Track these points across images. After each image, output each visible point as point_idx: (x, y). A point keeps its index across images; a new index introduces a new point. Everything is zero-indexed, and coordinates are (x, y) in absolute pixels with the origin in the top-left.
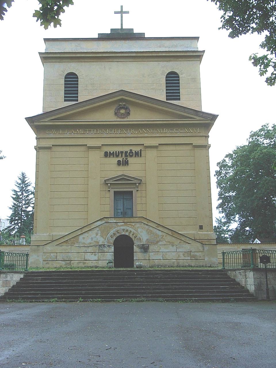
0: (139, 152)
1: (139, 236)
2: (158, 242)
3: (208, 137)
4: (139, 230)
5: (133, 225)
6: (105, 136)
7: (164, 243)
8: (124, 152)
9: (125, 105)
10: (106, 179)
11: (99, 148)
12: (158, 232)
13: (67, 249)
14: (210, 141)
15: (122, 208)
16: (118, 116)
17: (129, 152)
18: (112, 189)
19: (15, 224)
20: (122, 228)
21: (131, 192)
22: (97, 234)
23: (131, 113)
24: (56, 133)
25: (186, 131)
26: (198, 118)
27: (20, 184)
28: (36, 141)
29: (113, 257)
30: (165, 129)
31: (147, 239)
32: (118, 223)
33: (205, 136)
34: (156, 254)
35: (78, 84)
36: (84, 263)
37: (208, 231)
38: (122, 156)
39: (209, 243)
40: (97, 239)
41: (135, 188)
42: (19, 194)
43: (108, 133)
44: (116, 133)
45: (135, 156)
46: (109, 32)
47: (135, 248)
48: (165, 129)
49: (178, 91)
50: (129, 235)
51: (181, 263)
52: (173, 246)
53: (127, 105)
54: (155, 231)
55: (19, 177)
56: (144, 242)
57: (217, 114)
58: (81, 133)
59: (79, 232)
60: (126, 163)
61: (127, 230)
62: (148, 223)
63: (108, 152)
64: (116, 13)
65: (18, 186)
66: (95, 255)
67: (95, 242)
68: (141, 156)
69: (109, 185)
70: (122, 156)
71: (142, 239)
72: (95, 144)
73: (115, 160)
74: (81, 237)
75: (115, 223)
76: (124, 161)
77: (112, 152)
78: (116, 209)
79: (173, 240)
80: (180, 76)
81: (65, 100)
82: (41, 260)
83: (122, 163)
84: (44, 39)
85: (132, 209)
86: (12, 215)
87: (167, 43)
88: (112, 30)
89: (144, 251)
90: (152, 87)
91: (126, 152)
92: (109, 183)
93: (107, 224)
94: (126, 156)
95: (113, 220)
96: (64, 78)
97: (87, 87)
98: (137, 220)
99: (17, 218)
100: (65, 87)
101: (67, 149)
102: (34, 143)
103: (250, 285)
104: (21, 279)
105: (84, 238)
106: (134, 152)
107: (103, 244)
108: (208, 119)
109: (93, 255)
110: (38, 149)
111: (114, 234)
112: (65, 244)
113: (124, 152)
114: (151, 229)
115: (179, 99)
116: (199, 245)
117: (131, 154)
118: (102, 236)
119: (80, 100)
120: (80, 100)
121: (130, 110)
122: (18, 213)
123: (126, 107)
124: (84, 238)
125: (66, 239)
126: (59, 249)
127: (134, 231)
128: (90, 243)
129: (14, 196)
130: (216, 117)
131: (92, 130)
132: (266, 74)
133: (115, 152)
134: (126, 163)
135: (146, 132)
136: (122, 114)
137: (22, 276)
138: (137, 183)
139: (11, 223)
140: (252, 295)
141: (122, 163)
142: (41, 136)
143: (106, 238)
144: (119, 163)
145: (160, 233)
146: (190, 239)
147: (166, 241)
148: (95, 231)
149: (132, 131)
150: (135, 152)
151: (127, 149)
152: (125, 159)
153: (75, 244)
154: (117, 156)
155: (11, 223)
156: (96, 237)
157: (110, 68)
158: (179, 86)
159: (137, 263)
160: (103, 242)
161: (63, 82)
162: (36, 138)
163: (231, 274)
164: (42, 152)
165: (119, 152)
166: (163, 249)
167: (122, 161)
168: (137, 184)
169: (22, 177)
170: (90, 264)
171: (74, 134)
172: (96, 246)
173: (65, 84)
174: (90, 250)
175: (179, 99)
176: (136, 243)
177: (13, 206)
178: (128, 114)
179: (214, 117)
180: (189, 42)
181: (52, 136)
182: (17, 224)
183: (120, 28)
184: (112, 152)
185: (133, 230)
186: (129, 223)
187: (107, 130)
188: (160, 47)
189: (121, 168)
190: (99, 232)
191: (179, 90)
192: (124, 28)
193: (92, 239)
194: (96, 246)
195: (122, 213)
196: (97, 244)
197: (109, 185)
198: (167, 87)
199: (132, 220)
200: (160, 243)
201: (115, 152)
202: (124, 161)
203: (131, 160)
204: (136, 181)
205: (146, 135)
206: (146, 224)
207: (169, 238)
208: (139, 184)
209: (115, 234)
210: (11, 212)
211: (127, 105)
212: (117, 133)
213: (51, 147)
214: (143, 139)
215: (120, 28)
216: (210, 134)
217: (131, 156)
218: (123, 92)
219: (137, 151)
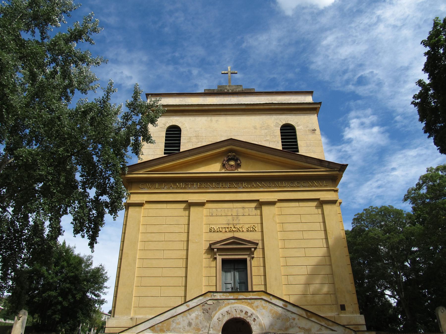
9: (235, 156)
10: (211, 242)
16: (226, 168)
18: (220, 256)
21: (245, 261)
23: (242, 164)
24: (150, 187)
30: (284, 182)
43: (214, 187)
44: (224, 186)
48: (284, 182)
49: (297, 150)
53: (237, 156)
58: (181, 187)
72: (198, 200)
81: (164, 154)
89: (331, 242)
90: (265, 139)
92: (215, 248)
96: (165, 131)
97: (190, 139)
101: (164, 206)
108: (335, 170)
119: (181, 150)
120: (181, 150)
121: (241, 161)
123: (236, 158)
130: (346, 167)
131: (195, 183)
132: (420, 83)
138: (253, 248)
146: (162, 323)
149: (244, 185)
157: (217, 121)
161: (164, 135)
168: (252, 249)
173: (166, 137)
204: (249, 246)
211: (237, 156)
212: (226, 186)
213: (143, 203)
218: (231, 141)
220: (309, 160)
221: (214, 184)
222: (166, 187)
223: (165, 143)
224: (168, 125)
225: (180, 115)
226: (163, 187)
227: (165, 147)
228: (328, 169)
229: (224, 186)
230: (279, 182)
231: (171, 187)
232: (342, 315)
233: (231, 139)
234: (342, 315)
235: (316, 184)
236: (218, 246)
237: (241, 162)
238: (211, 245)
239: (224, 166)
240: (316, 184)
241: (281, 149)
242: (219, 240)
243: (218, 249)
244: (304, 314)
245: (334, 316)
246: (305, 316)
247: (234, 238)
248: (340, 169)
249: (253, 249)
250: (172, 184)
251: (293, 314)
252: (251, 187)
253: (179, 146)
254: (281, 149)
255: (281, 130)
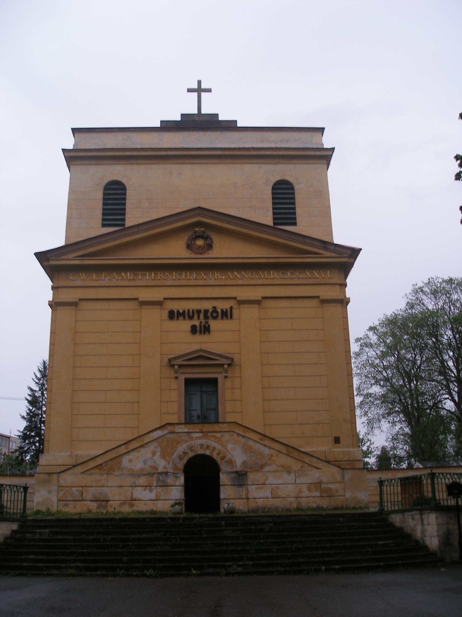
0: (229, 310)
1: (228, 457)
2: (262, 467)
3: (345, 285)
4: (230, 446)
5: (218, 438)
6: (170, 283)
7: (274, 467)
8: (203, 311)
9: (204, 232)
11: (159, 303)
12: (262, 448)
13: (100, 480)
14: (349, 292)
15: (198, 408)
16: (192, 251)
17: (210, 311)
19: (30, 443)
20: (199, 442)
21: (214, 382)
22: (154, 454)
24: (85, 278)
25: (308, 276)
26: (327, 254)
27: (39, 379)
28: (52, 292)
29: (183, 494)
30: (272, 272)
31: (244, 462)
32: (192, 434)
33: (341, 285)
34: (259, 488)
35: (125, 199)
36: (132, 505)
37: (348, 447)
38: (199, 317)
39: (351, 467)
40: (155, 462)
41: (221, 373)
42: (38, 394)
45: (222, 318)
46: (179, 118)
47: (224, 478)
50: (211, 455)
51: (304, 502)
52: (289, 472)
53: (208, 233)
54: (258, 447)
55: (39, 368)
56: (238, 466)
57: (361, 248)
59: (123, 450)
60: (206, 330)
61: (208, 446)
62: (244, 432)
63: (176, 311)
64: (189, 90)
65: (37, 381)
66: (151, 491)
67: (151, 467)
68: (231, 317)
69: (176, 367)
70: (199, 317)
71: (234, 463)
73: (186, 325)
74: (125, 460)
75: (186, 434)
76: (202, 325)
77: (181, 311)
78: (188, 410)
79: (289, 461)
80: (296, 187)
81: (104, 225)
82: (55, 499)
83: (198, 329)
84: (72, 129)
85: (216, 410)
86: (26, 428)
87: (273, 136)
88: (183, 115)
91: (206, 311)
92: (176, 365)
93: (172, 436)
94: (206, 317)
95: (182, 428)
98: (225, 427)
99: (33, 434)
100: (104, 204)
101: (105, 305)
102: (49, 296)
103: (431, 537)
104: (13, 531)
105: (130, 461)
106: (219, 311)
107: (166, 471)
109: (147, 491)
110: (53, 305)
111: (185, 453)
112: (97, 471)
113: (203, 311)
114: (251, 443)
115: (295, 224)
116: (335, 470)
117: (215, 315)
118: (163, 456)
119: (128, 223)
120: (128, 223)
122: (36, 427)
124: (130, 461)
125: (99, 461)
126: (87, 480)
127: (220, 447)
128: (142, 470)
129: (30, 398)
131: (148, 273)
133: (186, 311)
134: (206, 330)
135: (239, 277)
136: (200, 247)
137: (15, 526)
138: (226, 364)
139: (24, 442)
140: (434, 554)
141: (198, 329)
142: (62, 283)
143: (170, 460)
144: (194, 330)
145: (266, 451)
147: (277, 465)
148: (152, 447)
149: (216, 277)
150: (222, 310)
151: (208, 305)
152: (203, 322)
153: (114, 471)
154: (191, 318)
155: (24, 442)
156: (152, 459)
158: (294, 203)
159: (224, 506)
160: (165, 468)
162: (53, 288)
163: (367, 442)
164: (61, 310)
165: (193, 311)
166: (272, 480)
167: (198, 326)
169: (42, 367)
170: (141, 507)
171: (117, 280)
172: (151, 475)
174: (142, 481)
175: (295, 224)
176: (224, 467)
177: (28, 414)
178: (210, 247)
179: (333, 149)
180: (308, 135)
181: (79, 283)
182: (34, 443)
183: (196, 112)
184: (181, 311)
185: (218, 447)
186: (213, 434)
187: (173, 273)
188: (262, 141)
189: (198, 338)
190: (159, 449)
191: (294, 209)
192: (203, 112)
193: (145, 462)
194: (151, 475)
195: (198, 417)
196: (154, 471)
197: (176, 367)
198: (273, 204)
199: (216, 427)
200: (267, 468)
201: (186, 311)
202: (202, 325)
203: (213, 324)
204: (223, 361)
205: (240, 282)
206: (241, 435)
207: (284, 460)
208: (229, 365)
209: (186, 453)
210: (24, 424)
211: (208, 233)
214: (235, 288)
215: (196, 112)
216: (348, 280)
217: (215, 318)
219: (225, 310)
220: (307, 241)
221: (174, 274)
222: (106, 279)
223: (104, 209)
224: (106, 181)
225: (122, 164)
226: (103, 278)
227: (104, 214)
228: (334, 255)
229: (188, 277)
230: (266, 272)
231: (114, 279)
232: (335, 450)
233: (199, 208)
234: (335, 450)
235: (316, 274)
236: (179, 362)
237: (212, 242)
238: (170, 360)
239: (189, 247)
240: (316, 274)
241: (272, 225)
242: (182, 353)
243: (180, 366)
244: (284, 450)
245: (325, 451)
246: (285, 452)
247: (200, 350)
248: (350, 255)
249: (226, 366)
250: (115, 274)
251: (271, 450)
252: (226, 279)
253: (124, 220)
254: (272, 225)
255: (273, 189)
